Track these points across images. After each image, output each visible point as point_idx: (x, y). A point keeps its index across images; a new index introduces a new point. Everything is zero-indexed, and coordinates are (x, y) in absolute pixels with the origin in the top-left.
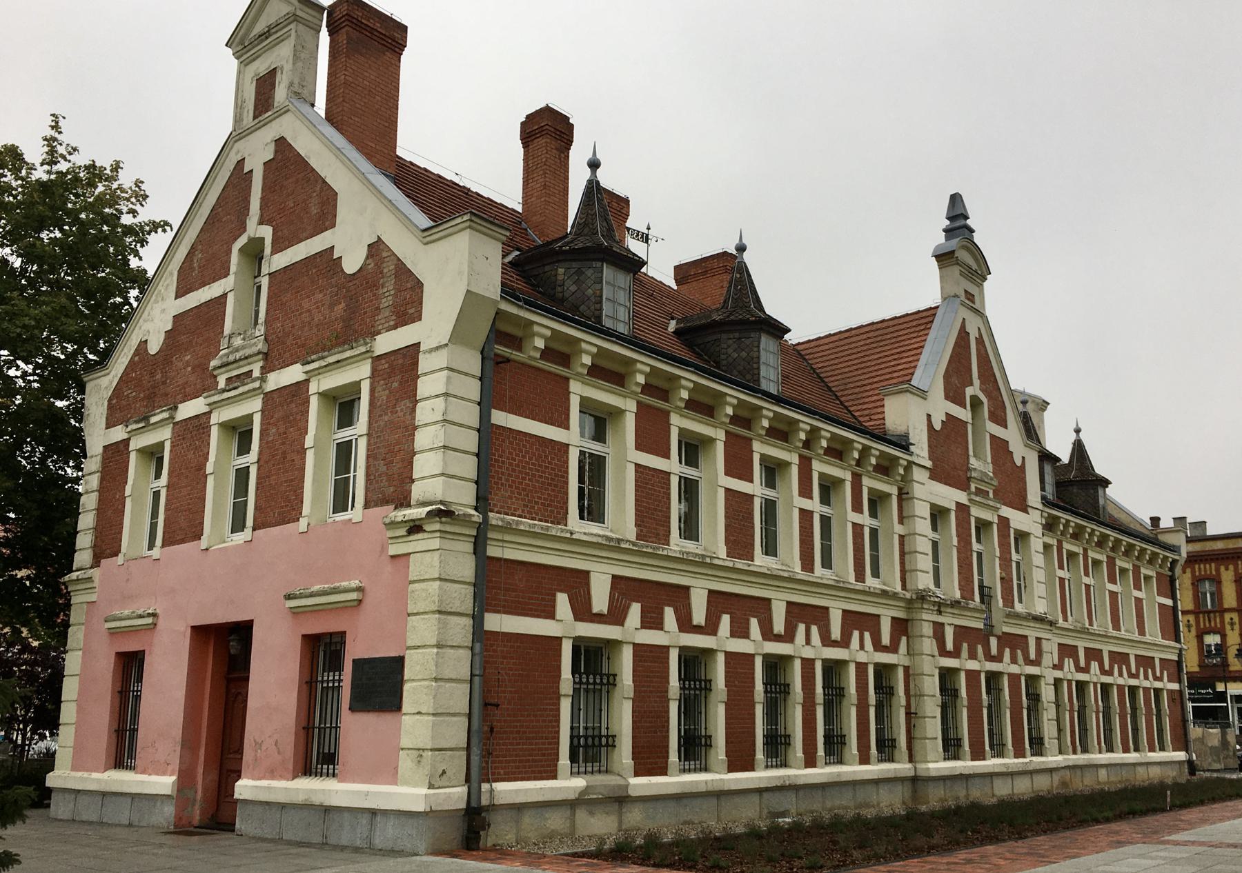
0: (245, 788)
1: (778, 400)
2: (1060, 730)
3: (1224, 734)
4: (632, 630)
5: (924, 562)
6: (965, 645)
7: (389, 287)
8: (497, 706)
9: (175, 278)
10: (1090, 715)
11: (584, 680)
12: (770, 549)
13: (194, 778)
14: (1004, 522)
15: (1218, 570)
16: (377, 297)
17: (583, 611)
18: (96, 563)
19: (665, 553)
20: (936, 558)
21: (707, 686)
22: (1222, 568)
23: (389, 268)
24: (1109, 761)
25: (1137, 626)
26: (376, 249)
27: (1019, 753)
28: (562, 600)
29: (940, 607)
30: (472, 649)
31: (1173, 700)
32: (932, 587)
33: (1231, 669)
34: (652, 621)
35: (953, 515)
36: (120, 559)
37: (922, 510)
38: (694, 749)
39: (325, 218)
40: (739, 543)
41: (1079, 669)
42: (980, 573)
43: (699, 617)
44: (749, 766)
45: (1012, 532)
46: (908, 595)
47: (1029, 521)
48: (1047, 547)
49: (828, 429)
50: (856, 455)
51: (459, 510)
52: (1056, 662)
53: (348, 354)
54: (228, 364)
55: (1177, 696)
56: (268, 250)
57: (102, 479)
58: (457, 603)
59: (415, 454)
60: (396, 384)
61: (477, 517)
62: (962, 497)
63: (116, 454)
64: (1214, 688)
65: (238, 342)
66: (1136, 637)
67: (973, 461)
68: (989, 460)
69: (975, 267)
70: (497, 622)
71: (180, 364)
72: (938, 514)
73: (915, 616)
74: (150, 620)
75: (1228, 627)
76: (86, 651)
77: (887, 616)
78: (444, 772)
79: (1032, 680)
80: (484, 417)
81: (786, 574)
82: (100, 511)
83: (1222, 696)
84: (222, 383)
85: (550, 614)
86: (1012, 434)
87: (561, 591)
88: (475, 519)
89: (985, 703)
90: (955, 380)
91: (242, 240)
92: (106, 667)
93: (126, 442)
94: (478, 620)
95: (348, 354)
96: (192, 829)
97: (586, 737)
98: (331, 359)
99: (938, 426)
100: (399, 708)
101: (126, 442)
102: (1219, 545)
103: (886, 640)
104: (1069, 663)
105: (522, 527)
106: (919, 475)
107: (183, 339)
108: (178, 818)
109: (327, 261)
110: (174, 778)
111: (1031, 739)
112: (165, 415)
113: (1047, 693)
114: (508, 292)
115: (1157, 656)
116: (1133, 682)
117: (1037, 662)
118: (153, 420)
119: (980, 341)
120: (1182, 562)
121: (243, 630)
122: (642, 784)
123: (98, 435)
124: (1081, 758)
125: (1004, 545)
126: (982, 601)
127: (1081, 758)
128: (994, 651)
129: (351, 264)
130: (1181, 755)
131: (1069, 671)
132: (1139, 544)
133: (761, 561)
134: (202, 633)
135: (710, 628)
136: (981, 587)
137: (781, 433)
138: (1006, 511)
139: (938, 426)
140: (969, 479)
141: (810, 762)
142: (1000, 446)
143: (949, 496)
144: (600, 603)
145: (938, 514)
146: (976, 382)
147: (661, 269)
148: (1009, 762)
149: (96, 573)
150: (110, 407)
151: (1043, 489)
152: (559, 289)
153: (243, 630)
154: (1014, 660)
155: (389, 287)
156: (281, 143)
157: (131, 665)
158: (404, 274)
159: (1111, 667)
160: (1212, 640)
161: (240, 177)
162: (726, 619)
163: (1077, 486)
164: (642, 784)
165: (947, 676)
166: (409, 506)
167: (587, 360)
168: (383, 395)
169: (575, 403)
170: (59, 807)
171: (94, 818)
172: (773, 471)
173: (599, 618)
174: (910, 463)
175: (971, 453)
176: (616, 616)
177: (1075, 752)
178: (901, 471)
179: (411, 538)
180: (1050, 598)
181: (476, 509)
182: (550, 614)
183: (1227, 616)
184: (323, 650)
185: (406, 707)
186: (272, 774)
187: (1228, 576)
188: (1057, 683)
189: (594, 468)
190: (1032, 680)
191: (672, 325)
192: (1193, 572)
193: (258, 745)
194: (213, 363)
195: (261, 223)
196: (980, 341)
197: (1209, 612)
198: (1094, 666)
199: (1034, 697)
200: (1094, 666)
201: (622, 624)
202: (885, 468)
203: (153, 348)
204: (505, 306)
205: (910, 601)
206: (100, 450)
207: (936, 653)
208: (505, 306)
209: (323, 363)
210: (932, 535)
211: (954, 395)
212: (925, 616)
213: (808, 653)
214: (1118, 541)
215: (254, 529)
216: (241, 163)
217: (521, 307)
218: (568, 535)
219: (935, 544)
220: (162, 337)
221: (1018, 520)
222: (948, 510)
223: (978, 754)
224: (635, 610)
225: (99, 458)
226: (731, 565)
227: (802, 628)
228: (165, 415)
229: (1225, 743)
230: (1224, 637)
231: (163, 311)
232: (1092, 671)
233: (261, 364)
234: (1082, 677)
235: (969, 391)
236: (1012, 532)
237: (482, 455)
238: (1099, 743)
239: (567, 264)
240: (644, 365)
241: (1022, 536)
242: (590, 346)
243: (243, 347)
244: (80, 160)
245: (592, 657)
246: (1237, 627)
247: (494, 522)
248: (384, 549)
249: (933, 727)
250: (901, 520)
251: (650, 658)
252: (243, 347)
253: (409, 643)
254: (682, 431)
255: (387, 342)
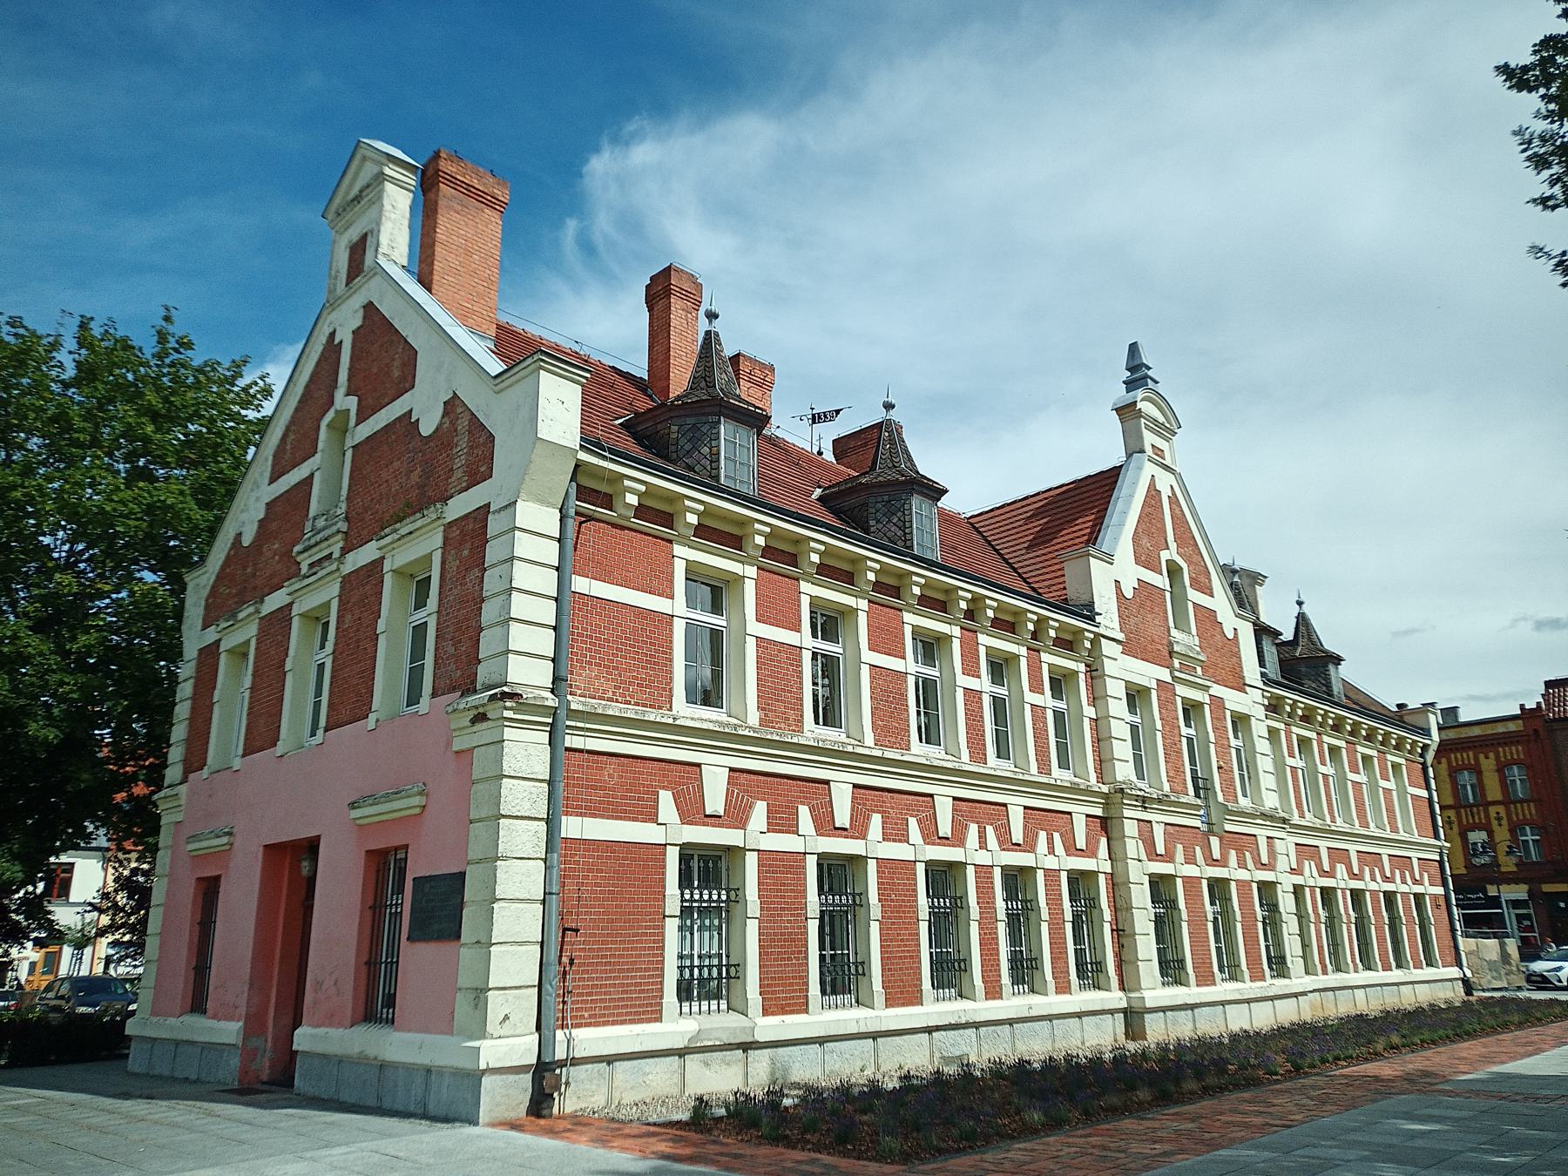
0: (304, 1038)
1: (931, 565)
2: (1305, 946)
3: (1502, 946)
4: (757, 834)
5: (1122, 750)
6: (1180, 847)
7: (463, 443)
8: (577, 931)
9: (270, 463)
10: (1354, 926)
11: (697, 897)
12: (929, 735)
13: (264, 1025)
14: (1217, 703)
15: (1476, 759)
16: (451, 458)
17: (692, 811)
18: (184, 780)
19: (795, 740)
20: (1136, 745)
21: (859, 901)
22: (1482, 756)
23: (463, 424)
24: (1369, 988)
25: (1393, 831)
26: (453, 405)
27: (1257, 976)
28: (666, 799)
29: (1144, 802)
30: (545, 861)
31: (1438, 906)
32: (1134, 778)
33: (1503, 869)
34: (782, 822)
35: (1154, 694)
36: (205, 772)
37: (1116, 689)
38: (841, 978)
39: (406, 382)
40: (890, 728)
41: (1323, 873)
42: (1193, 762)
43: (843, 817)
44: (915, 999)
45: (1228, 713)
46: (1105, 789)
47: (1250, 702)
48: (1273, 733)
49: (994, 598)
50: (1031, 626)
51: (528, 694)
52: (1294, 866)
53: (419, 523)
54: (311, 547)
55: (1442, 902)
56: (353, 422)
57: (196, 686)
58: (527, 805)
59: (482, 630)
60: (466, 552)
61: (552, 701)
62: (1165, 675)
63: (209, 654)
64: (1485, 892)
65: (321, 523)
66: (1388, 834)
67: (1174, 632)
68: (1194, 631)
69: (1161, 419)
70: (573, 827)
71: (269, 554)
72: (1136, 696)
73: (1113, 813)
74: (225, 840)
75: (1495, 823)
76: (171, 876)
77: (1080, 813)
78: (506, 1017)
79: (1267, 888)
80: (562, 584)
81: (949, 765)
82: (192, 720)
83: (1495, 902)
84: (304, 569)
85: (651, 816)
86: (1221, 603)
87: (663, 788)
88: (550, 703)
89: (1210, 917)
90: (1145, 542)
91: (330, 415)
92: (188, 893)
93: (217, 643)
94: (551, 822)
95: (419, 523)
96: (259, 1087)
97: (701, 968)
98: (404, 531)
99: (1129, 594)
100: (459, 937)
101: (217, 643)
102: (1476, 731)
103: (1018, 835)
104: (1309, 867)
105: (610, 712)
106: (1107, 648)
107: (274, 526)
108: (244, 1071)
109: (407, 423)
110: (241, 1023)
111: (1269, 958)
112: (251, 609)
113: (1286, 903)
114: (590, 442)
115: (1414, 855)
116: (1389, 887)
117: (1270, 867)
118: (241, 616)
119: (1173, 499)
120: (1434, 747)
121: (311, 847)
122: (770, 1027)
123: (193, 639)
124: (1334, 979)
125: (1219, 729)
126: (1197, 795)
127: (1334, 979)
128: (1216, 854)
129: (426, 429)
130: (1454, 972)
131: (1311, 878)
132: (1383, 728)
133: (919, 750)
134: (274, 851)
135: (858, 829)
136: (1195, 779)
137: (936, 603)
138: (1217, 690)
139: (1129, 594)
140: (1171, 653)
141: (993, 992)
142: (1208, 618)
143: (1148, 673)
144: (715, 801)
145: (1136, 696)
146: (1173, 545)
147: (789, 427)
148: (1247, 988)
149: (183, 789)
150: (207, 607)
151: (1262, 663)
152: (673, 448)
153: (311, 847)
154: (1242, 865)
155: (463, 443)
156: (369, 308)
157: (209, 889)
158: (476, 425)
159: (1361, 870)
160: (1477, 837)
161: (332, 348)
162: (876, 819)
163: (1302, 664)
164: (770, 1027)
165: (1160, 887)
166: (475, 692)
167: (692, 519)
168: (453, 565)
169: (680, 569)
170: (136, 1060)
171: (167, 1073)
172: (930, 647)
173: (713, 819)
174: (1097, 635)
175: (1171, 624)
176: (736, 816)
177: (1325, 972)
178: (1088, 644)
179: (475, 729)
180: (1282, 789)
181: (552, 692)
182: (651, 816)
183: (1493, 810)
184: (385, 865)
185: (466, 935)
186: (330, 1020)
187: (1488, 764)
188: (1298, 891)
189: (713, 647)
190: (1267, 888)
191: (818, 492)
192: (1449, 762)
193: (319, 984)
194: (296, 549)
195: (348, 394)
196: (1173, 499)
197: (1471, 806)
198: (1341, 869)
199: (1272, 907)
200: (1341, 869)
201: (864, 838)
202: (1067, 644)
203: (246, 542)
204: (583, 456)
205: (1106, 796)
206: (195, 654)
207: (1144, 857)
208: (583, 456)
209: (396, 536)
210: (1128, 717)
211: (1146, 559)
212: (1127, 813)
213: (983, 858)
214: (1356, 725)
215: (326, 730)
216: (332, 335)
217: (604, 458)
218: (670, 721)
219: (1134, 729)
220: (256, 526)
221: (1235, 701)
222: (1149, 689)
223: (1205, 979)
224: (760, 809)
225: (193, 663)
226: (879, 753)
227: (973, 828)
228: (251, 609)
229: (1505, 957)
230: (1490, 834)
231: (258, 499)
232: (1339, 876)
233: (341, 544)
234: (1327, 882)
235: (1165, 555)
236: (1228, 713)
237: (564, 631)
238: (1353, 961)
239: (680, 422)
240: (763, 525)
241: (1241, 721)
242: (695, 503)
243: (325, 528)
244: (197, 358)
245: (707, 867)
246: (1505, 822)
247: (573, 706)
248: (449, 743)
249: (1146, 946)
250: (1094, 701)
251: (780, 867)
252: (325, 528)
253: (471, 856)
254: (814, 601)
255: (460, 506)
